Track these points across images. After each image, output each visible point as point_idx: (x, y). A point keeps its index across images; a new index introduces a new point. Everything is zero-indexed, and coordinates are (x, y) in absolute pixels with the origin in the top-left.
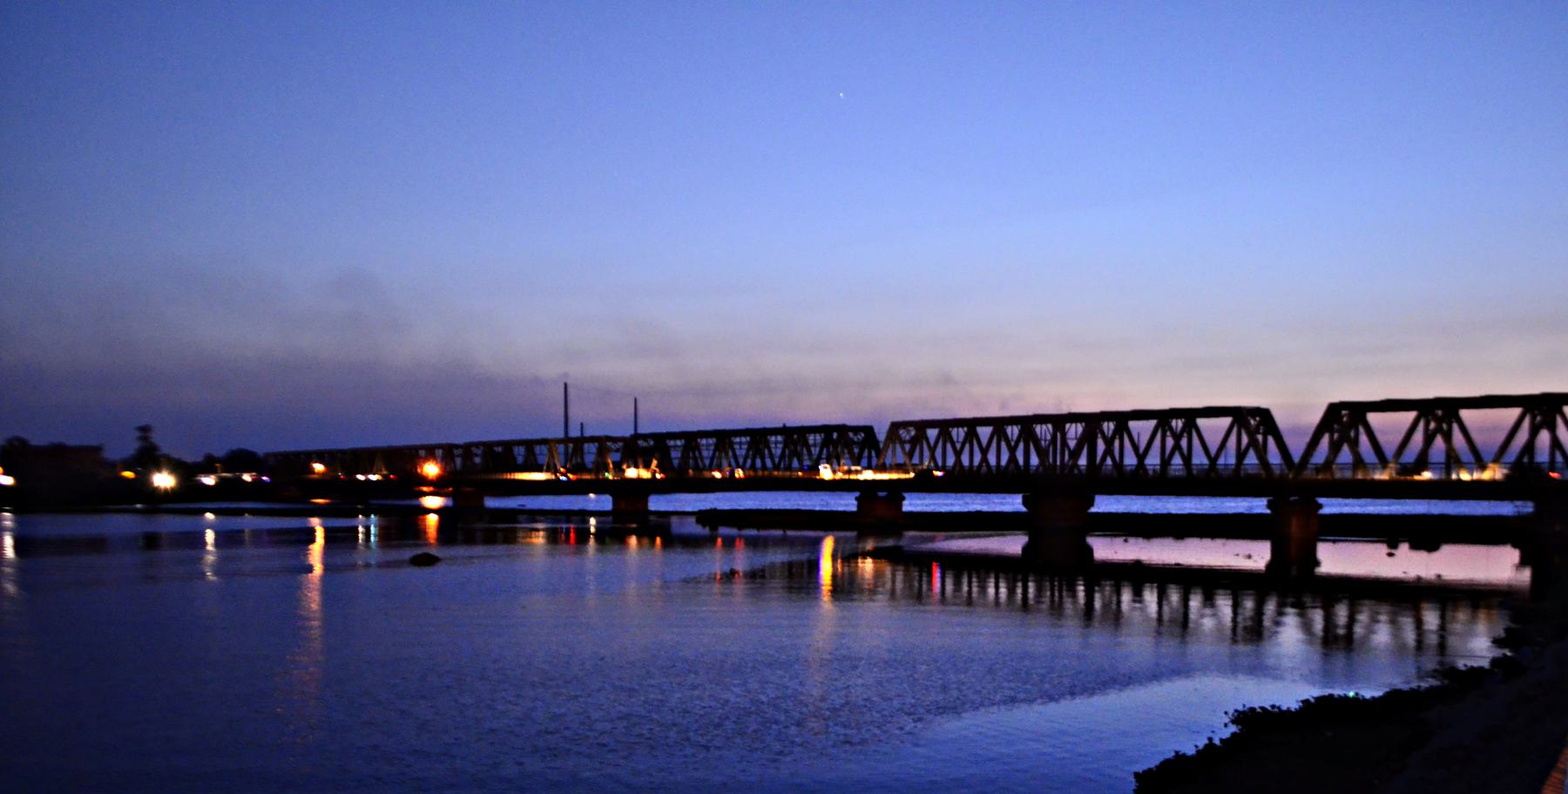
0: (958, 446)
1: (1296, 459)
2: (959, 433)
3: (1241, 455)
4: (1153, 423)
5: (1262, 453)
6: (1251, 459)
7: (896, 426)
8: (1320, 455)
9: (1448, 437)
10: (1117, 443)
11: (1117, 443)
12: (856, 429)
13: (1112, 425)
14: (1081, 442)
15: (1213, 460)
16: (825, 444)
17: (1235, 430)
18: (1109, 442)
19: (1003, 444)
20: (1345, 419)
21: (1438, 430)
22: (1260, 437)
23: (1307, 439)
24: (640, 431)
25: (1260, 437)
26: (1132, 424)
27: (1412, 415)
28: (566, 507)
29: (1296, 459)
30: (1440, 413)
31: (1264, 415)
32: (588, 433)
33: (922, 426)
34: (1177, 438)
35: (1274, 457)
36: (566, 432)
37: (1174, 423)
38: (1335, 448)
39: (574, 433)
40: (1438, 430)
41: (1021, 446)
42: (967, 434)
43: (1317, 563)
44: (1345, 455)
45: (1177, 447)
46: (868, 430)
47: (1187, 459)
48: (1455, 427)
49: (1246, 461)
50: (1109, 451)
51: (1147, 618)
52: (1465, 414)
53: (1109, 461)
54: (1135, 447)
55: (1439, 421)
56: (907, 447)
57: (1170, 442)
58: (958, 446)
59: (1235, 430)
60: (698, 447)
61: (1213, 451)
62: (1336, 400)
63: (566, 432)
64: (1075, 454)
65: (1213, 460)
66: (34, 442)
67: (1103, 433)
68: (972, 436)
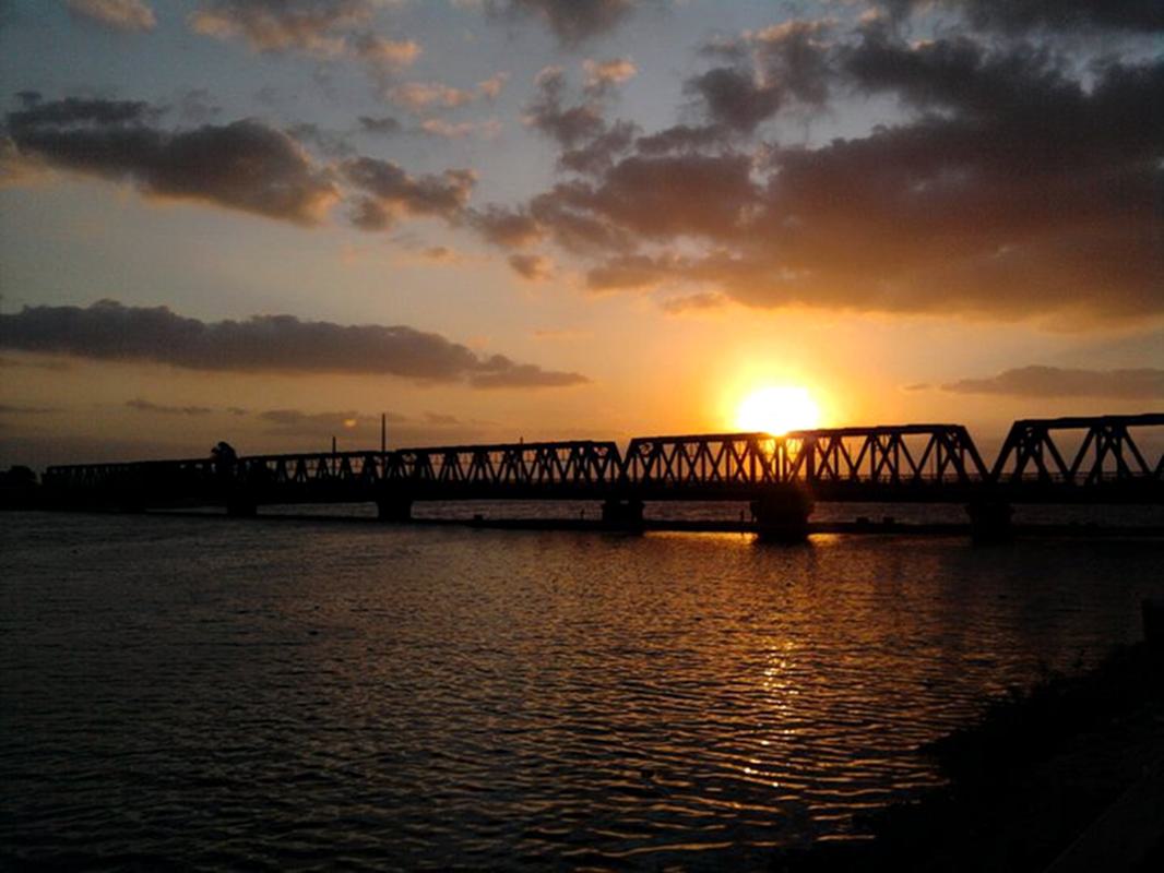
0: (692, 459)
1: (1069, 468)
2: (692, 449)
3: (941, 467)
4: (862, 439)
5: (959, 463)
6: (950, 469)
7: (636, 444)
8: (1010, 466)
9: (1118, 452)
10: (832, 456)
11: (832, 456)
12: (600, 445)
13: (828, 441)
14: (801, 456)
15: (854, 469)
16: (572, 458)
17: (935, 445)
18: (825, 456)
19: (684, 459)
20: (1028, 435)
21: (1109, 444)
22: (957, 451)
23: (998, 454)
24: (338, 450)
25: (957, 451)
26: (845, 441)
27: (1086, 431)
28: (547, 504)
29: (1069, 468)
30: (1110, 429)
31: (960, 431)
32: (525, 442)
33: (658, 443)
34: (885, 452)
35: (970, 467)
36: (384, 447)
37: (881, 439)
38: (1022, 461)
39: (391, 447)
40: (1109, 444)
41: (748, 459)
42: (699, 449)
43: (603, 507)
44: (1031, 468)
45: (885, 459)
46: (612, 446)
47: (895, 471)
48: (1124, 442)
49: (946, 472)
50: (825, 464)
51: (836, 547)
52: (1130, 430)
53: (824, 472)
54: (848, 458)
55: (1109, 437)
56: (646, 460)
57: (879, 456)
58: (692, 459)
59: (935, 445)
60: (427, 462)
61: (854, 462)
62: (1021, 418)
63: (384, 447)
64: (795, 467)
65: (917, 472)
66: (239, 320)
67: (879, 444)
68: (703, 449)
